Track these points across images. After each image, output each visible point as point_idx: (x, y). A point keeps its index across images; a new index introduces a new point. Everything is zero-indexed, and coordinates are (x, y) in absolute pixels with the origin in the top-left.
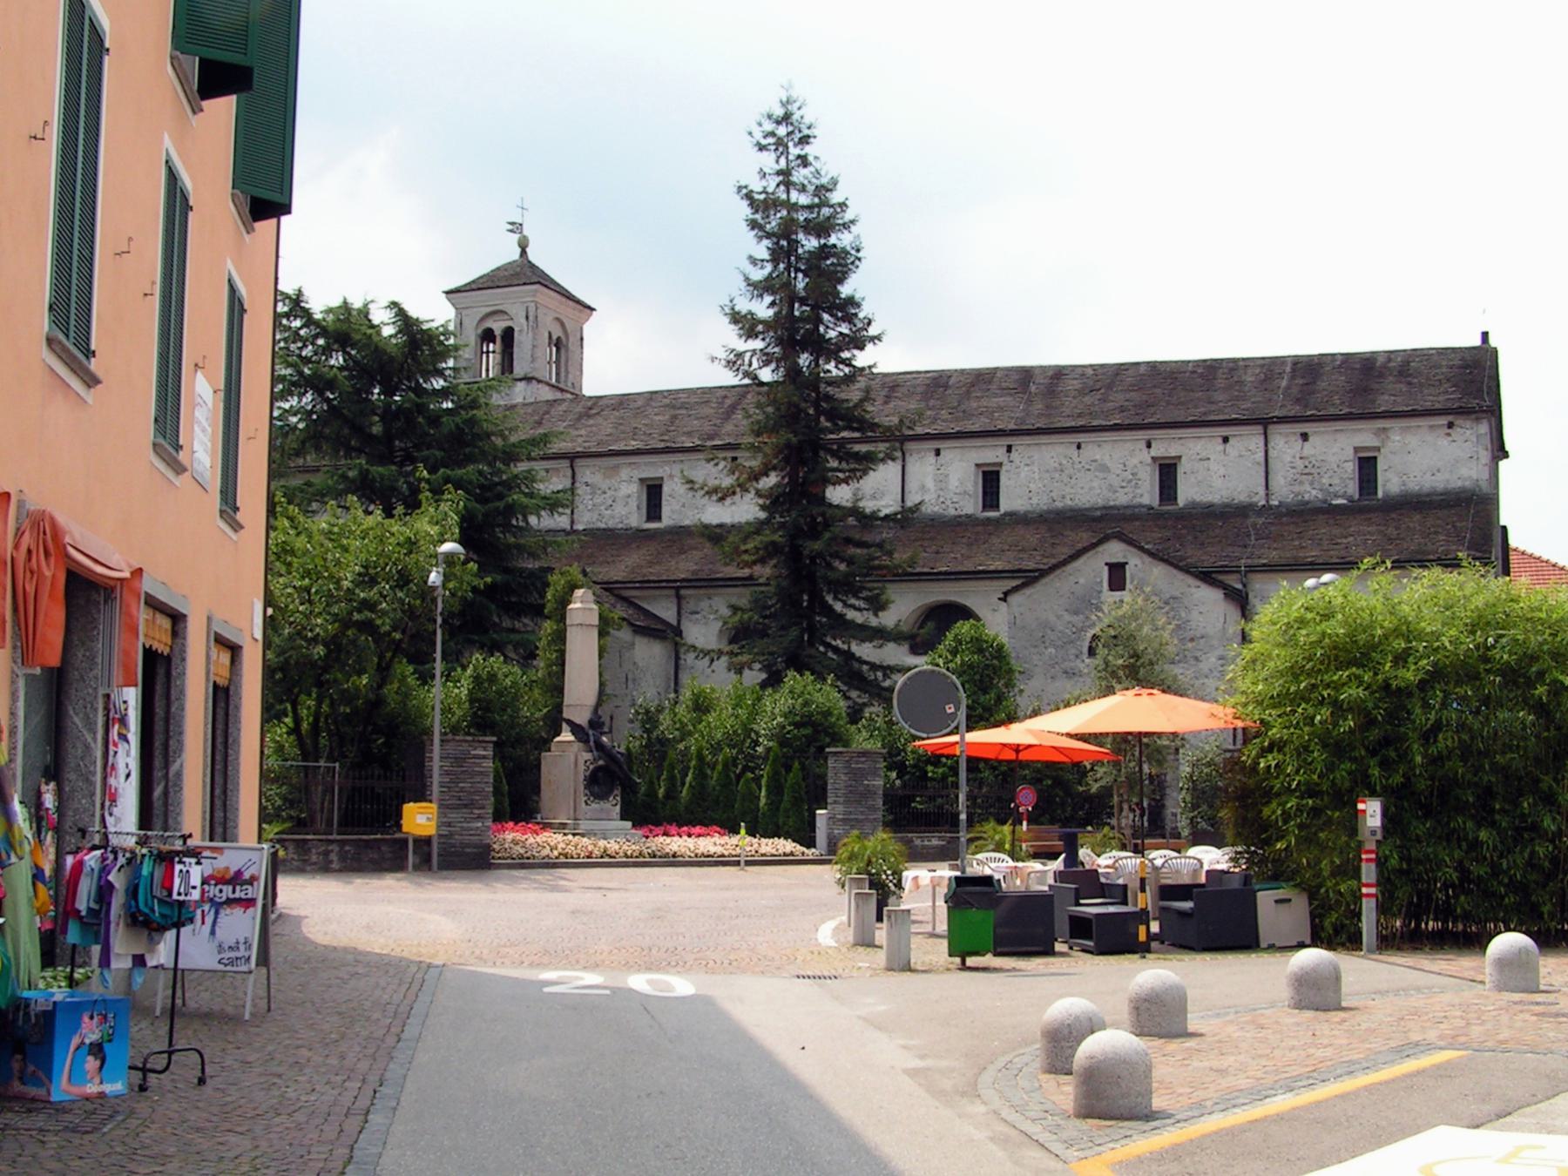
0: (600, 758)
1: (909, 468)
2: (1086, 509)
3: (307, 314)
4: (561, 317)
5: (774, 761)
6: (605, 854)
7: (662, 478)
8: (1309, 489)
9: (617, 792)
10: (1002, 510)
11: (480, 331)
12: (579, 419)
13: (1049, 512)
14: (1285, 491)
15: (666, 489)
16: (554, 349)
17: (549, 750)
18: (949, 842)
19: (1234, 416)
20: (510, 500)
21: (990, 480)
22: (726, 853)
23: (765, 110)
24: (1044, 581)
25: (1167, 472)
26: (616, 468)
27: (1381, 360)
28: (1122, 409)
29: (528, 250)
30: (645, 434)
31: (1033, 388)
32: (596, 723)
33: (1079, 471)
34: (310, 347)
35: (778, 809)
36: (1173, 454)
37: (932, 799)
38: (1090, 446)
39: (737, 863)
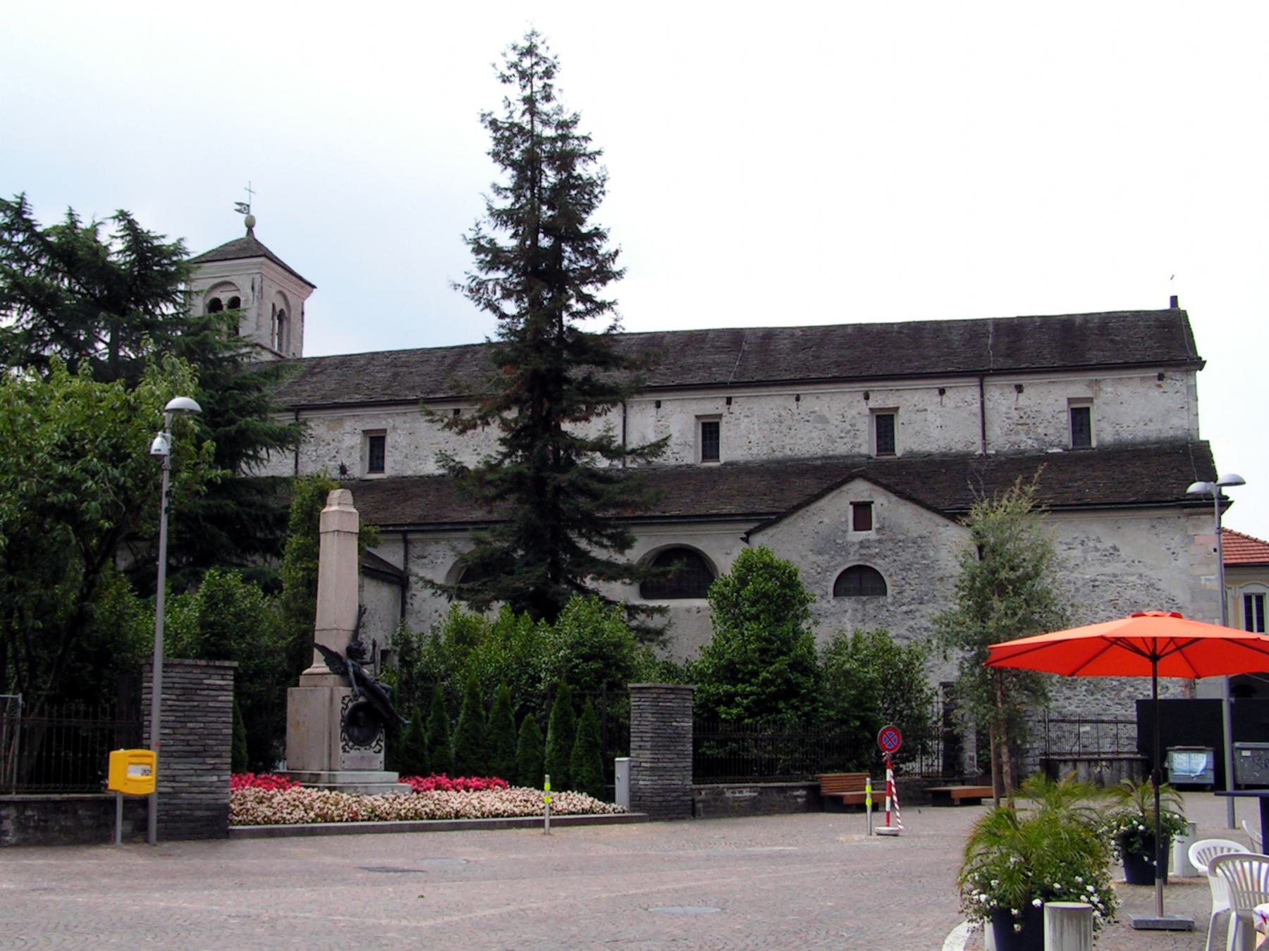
0: (362, 694)
1: (631, 420)
2: (808, 459)
3: (29, 226)
4: (285, 291)
5: (562, 700)
6: (374, 815)
7: (385, 430)
8: (1024, 438)
9: (381, 736)
10: (722, 459)
11: (208, 301)
12: (303, 376)
13: (769, 462)
14: (1001, 441)
15: (389, 441)
16: (277, 322)
17: (297, 685)
18: (760, 794)
19: (950, 369)
20: (243, 423)
21: (710, 431)
22: (517, 811)
23: (510, 42)
24: (787, 521)
25: (885, 423)
26: (341, 420)
27: (1078, 321)
28: (838, 364)
29: (254, 229)
30: (368, 388)
31: (745, 347)
32: (355, 651)
33: (798, 421)
34: (33, 267)
35: (568, 756)
36: (891, 406)
37: (722, 743)
38: (809, 398)
39: (540, 824)
